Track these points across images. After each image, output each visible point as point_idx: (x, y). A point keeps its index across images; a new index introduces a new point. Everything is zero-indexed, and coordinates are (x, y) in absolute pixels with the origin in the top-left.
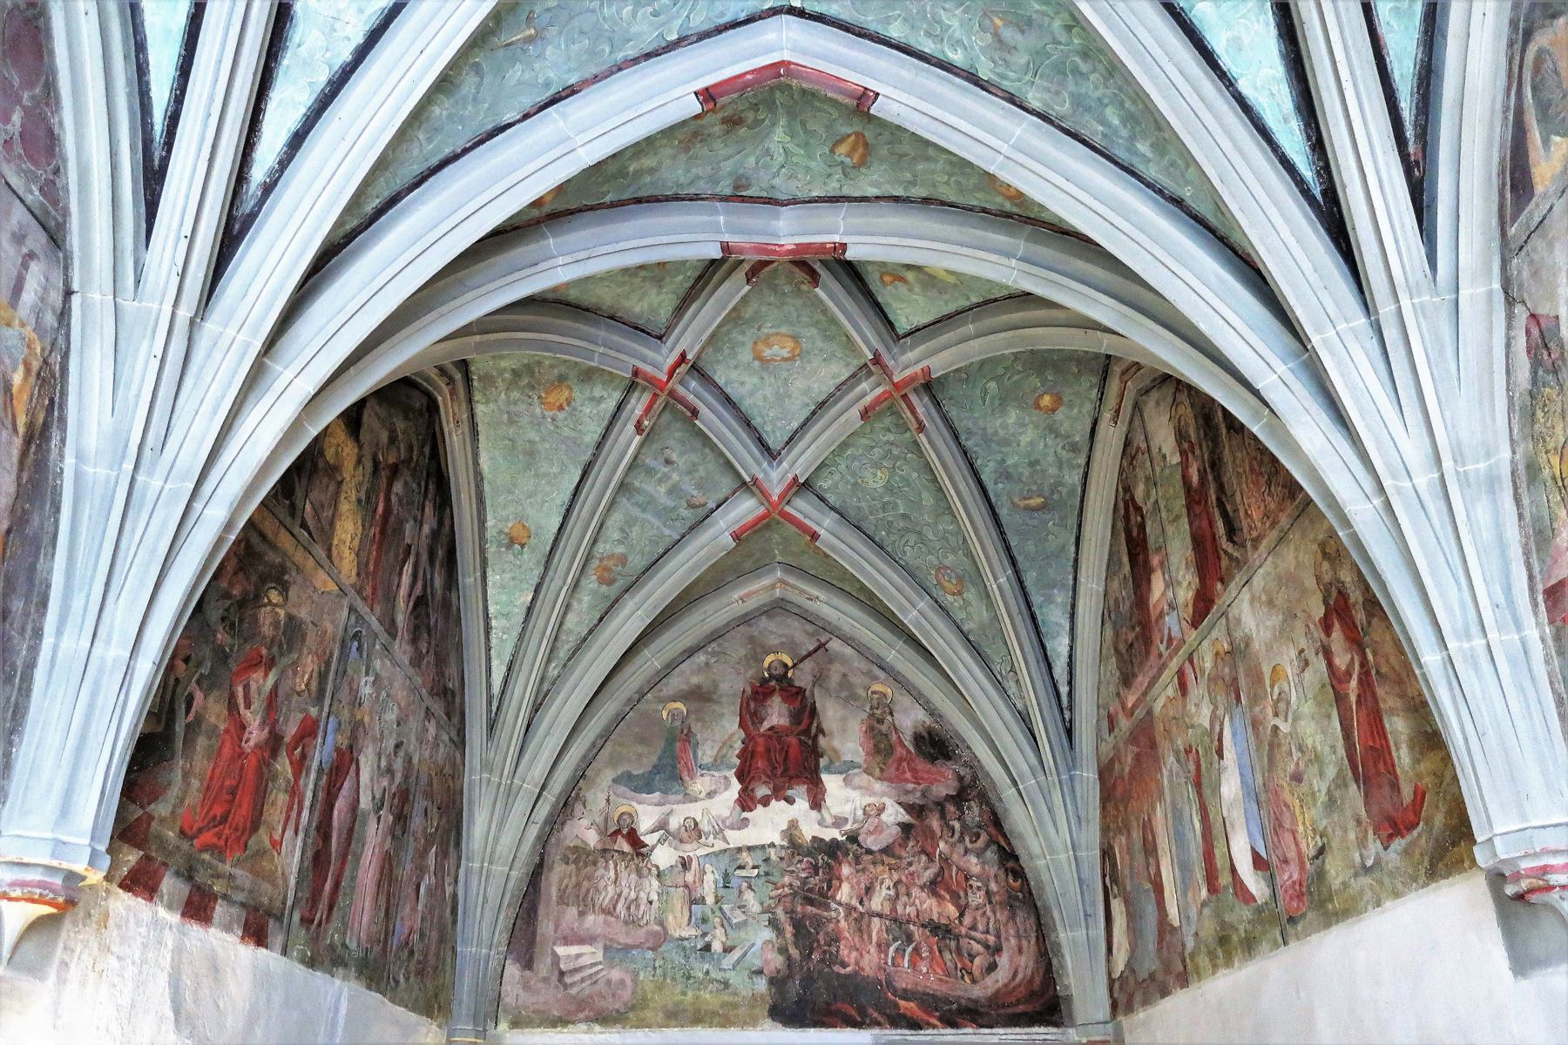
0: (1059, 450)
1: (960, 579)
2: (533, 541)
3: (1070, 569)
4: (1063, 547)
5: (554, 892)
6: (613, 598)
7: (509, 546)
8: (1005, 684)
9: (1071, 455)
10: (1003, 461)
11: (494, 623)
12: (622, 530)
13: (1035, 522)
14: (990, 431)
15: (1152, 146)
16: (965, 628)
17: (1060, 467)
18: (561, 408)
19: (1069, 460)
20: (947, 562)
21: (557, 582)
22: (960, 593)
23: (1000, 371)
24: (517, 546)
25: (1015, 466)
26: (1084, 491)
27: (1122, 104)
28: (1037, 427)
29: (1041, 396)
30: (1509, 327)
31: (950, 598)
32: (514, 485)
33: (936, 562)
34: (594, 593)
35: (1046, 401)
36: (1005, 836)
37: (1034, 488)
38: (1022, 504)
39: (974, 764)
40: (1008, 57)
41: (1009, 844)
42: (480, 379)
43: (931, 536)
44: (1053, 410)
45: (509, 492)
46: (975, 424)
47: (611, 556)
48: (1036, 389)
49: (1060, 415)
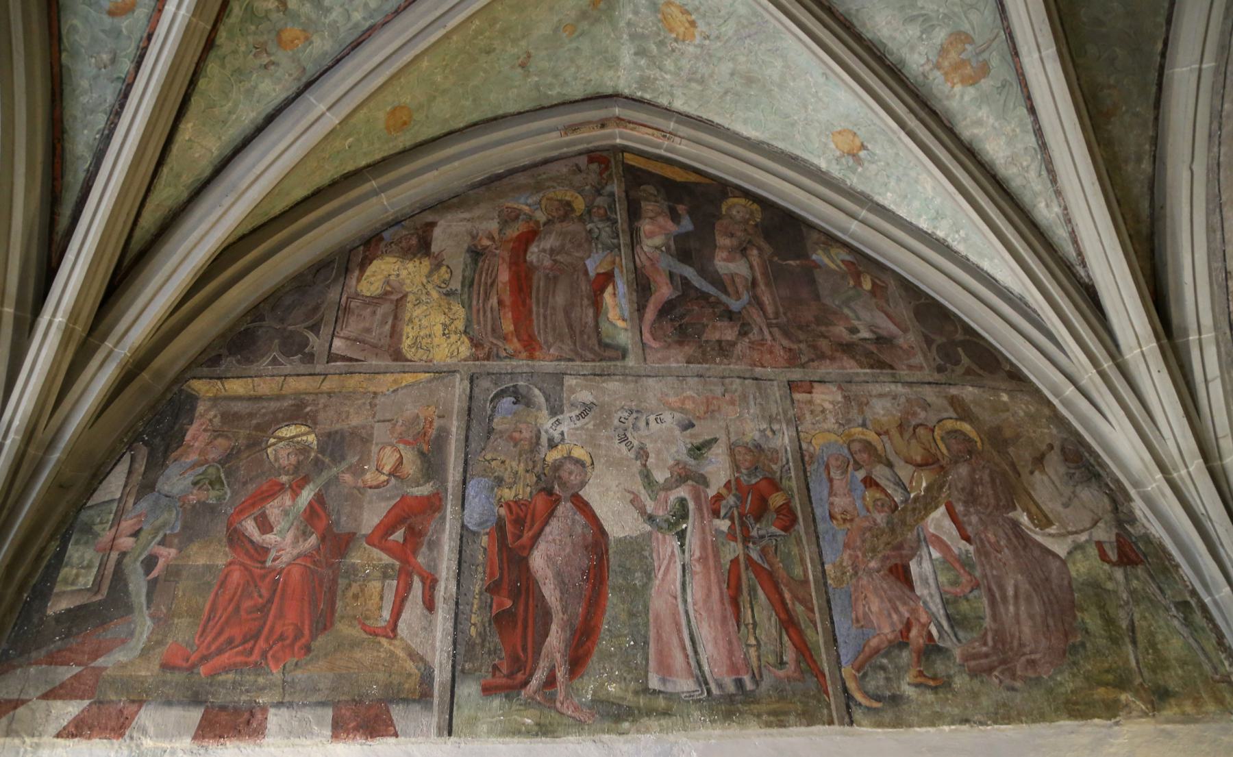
2: (862, 133)
5: (391, 145)
6: (1011, 77)
7: (859, 161)
11: (940, 234)
12: (912, 19)
18: (693, 24)
21: (684, 146)
24: (862, 154)
32: (787, 116)
34: (983, 99)
42: (644, 89)
45: (793, 125)
47: (943, 51)
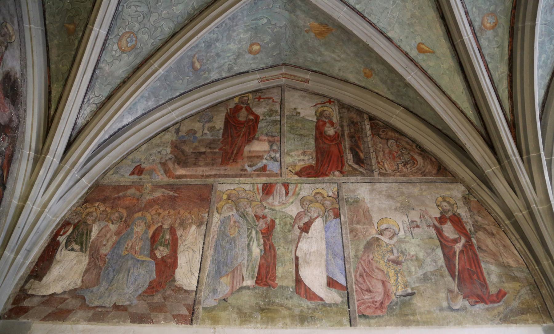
0: (227, 64)
1: (134, 47)
3: (167, 99)
4: (176, 90)
8: (85, 106)
9: (226, 70)
10: (217, 40)
13: (187, 70)
14: (235, 28)
15: (542, 74)
16: (101, 65)
17: (218, 68)
19: (223, 70)
20: (140, 36)
22: (123, 52)
23: (273, 23)
25: (216, 47)
26: (209, 83)
27: (548, 59)
28: (239, 49)
29: (259, 44)
30: (27, 165)
31: (116, 47)
33: (136, 29)
35: (256, 48)
36: (8, 172)
37: (205, 61)
38: (195, 60)
39: (21, 119)
40: (548, 12)
41: (7, 177)
43: (152, 19)
44: (251, 53)
46: (240, 19)
48: (263, 41)
49: (248, 56)
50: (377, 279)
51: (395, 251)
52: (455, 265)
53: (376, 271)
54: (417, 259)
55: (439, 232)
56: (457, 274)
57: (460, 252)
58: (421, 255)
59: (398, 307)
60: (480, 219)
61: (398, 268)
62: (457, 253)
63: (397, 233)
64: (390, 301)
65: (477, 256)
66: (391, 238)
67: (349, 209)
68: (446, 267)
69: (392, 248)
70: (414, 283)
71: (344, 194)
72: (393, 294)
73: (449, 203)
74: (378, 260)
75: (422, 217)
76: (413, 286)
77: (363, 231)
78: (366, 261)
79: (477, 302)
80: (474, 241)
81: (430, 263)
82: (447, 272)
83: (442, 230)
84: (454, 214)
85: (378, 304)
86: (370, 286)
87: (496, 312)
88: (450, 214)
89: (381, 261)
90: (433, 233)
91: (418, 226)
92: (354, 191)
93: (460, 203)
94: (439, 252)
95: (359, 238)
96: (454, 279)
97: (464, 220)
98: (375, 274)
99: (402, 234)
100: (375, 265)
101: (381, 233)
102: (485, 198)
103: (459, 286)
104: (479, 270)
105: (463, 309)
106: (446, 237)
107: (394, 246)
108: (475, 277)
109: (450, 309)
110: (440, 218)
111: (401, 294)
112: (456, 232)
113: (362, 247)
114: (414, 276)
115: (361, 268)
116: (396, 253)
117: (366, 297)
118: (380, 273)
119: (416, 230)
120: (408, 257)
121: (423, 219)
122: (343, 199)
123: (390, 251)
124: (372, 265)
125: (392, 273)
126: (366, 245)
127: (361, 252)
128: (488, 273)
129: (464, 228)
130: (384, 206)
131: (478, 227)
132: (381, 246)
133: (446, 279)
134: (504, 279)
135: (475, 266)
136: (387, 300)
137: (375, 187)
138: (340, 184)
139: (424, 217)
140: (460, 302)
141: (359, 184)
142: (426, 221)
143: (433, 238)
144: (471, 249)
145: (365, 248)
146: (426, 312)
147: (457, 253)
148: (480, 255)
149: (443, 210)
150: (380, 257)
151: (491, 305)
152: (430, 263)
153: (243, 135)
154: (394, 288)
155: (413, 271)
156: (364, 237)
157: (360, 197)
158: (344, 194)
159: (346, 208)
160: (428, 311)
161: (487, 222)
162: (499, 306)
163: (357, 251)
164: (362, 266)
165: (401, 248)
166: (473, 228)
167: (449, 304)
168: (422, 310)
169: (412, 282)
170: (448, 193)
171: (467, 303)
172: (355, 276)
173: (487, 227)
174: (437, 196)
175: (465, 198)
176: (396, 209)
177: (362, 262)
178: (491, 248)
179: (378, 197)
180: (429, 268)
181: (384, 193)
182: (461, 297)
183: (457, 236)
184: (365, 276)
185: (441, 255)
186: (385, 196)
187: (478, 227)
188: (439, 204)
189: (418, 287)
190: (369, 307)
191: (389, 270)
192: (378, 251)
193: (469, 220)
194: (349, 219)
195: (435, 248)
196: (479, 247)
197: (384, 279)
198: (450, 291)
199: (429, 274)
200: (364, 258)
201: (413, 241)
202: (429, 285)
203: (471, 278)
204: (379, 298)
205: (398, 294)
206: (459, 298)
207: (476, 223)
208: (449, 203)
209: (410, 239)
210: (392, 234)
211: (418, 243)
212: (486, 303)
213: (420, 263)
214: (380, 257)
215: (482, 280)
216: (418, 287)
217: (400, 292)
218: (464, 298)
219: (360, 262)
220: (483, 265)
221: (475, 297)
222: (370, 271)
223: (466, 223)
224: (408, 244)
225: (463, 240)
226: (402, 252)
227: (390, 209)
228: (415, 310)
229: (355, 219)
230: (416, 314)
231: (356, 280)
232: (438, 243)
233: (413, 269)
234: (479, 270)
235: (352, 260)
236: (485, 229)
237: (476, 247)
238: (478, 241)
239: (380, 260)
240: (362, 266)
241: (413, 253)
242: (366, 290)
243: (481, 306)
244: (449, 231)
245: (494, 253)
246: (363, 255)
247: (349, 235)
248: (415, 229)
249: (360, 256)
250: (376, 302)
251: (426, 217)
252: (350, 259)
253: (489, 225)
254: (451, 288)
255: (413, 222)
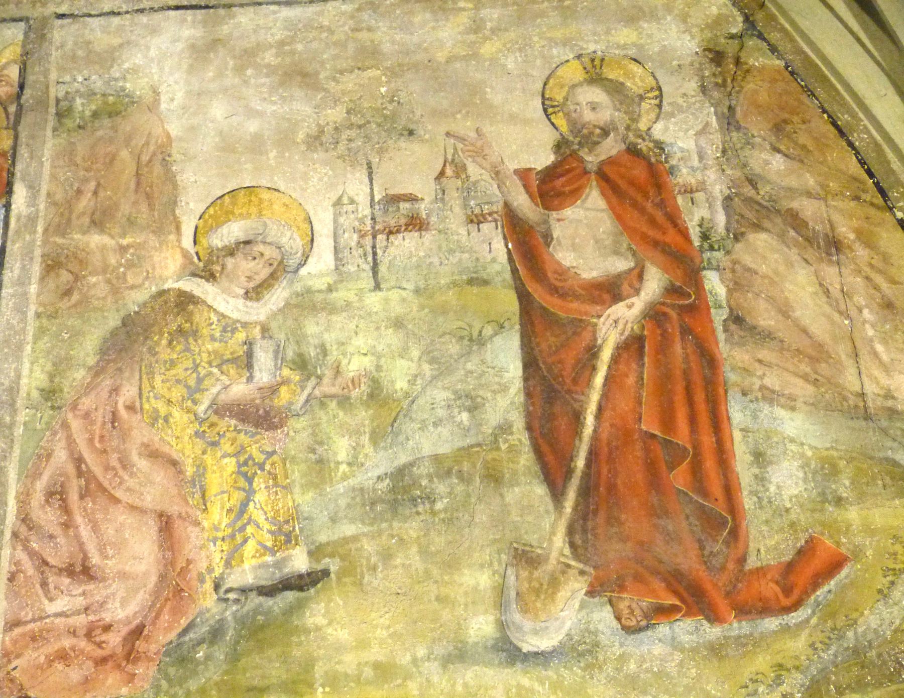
50: (133, 508)
51: (264, 359)
52: (577, 418)
53: (142, 464)
54: (376, 393)
55: (528, 246)
56: (580, 463)
57: (622, 349)
58: (399, 377)
59: (220, 654)
60: (777, 163)
61: (257, 445)
62: (606, 355)
63: (293, 262)
64: (184, 622)
65: (711, 361)
66: (255, 293)
67: (67, 154)
68: (529, 428)
69: (249, 344)
70: (334, 520)
71: (59, 78)
72: (209, 586)
73: (616, 89)
74: (163, 410)
75: (451, 170)
76: (323, 538)
77: (113, 260)
78: (99, 417)
79: (662, 612)
80: (715, 284)
81: (441, 413)
82: (526, 459)
83: (548, 237)
84: (633, 151)
85: (114, 640)
86: (91, 548)
87: (762, 662)
88: (611, 147)
89: (177, 415)
90: (494, 249)
91: (416, 224)
92: (105, 59)
93: (682, 88)
94: (506, 357)
95: (85, 301)
96: (557, 495)
97: (684, 176)
98: (131, 482)
99: (319, 267)
100: (140, 433)
101: (208, 269)
102: (829, 50)
103: (580, 532)
104: (707, 440)
105: (580, 650)
106: (562, 272)
107: (265, 330)
108: (679, 478)
109: (508, 651)
110: (549, 174)
111: (249, 579)
112: (625, 242)
113: (88, 349)
114: (341, 488)
115: (61, 455)
116: (265, 369)
117: (60, 604)
118: (161, 476)
119: (406, 245)
120: (327, 387)
121: (452, 184)
122: (42, 103)
123: (234, 360)
124: (125, 436)
125: (221, 472)
126: (114, 333)
127: (80, 374)
128: (759, 457)
129: (674, 220)
130: (253, 126)
131: (752, 208)
132: (195, 333)
133: (512, 495)
134: (844, 486)
135: (693, 420)
136: (166, 616)
137: (225, 29)
138: (44, 22)
139: (460, 170)
140: (571, 612)
141: (144, 19)
142: (469, 190)
143: (485, 283)
144: (686, 331)
145: (103, 351)
146: (368, 672)
147: (606, 355)
148: (732, 355)
149: (576, 127)
150: (177, 393)
151: (738, 627)
152: (441, 413)
153: (778, 597)
154: (217, 554)
155: (342, 456)
156: (115, 291)
157: (136, 86)
158: (53, 76)
159: (50, 145)
160: (377, 666)
161: (811, 181)
162: (786, 629)
163: (60, 366)
164: (71, 442)
165: (300, 338)
166: (721, 219)
167: (502, 626)
168: (349, 662)
169: (323, 518)
170: (625, 35)
171: (603, 617)
172: (24, 501)
173: (808, 208)
174: (559, 53)
175: (717, 57)
176: (315, 141)
177: (75, 424)
178: (806, 321)
179: (231, 80)
180: (429, 441)
181: (269, 57)
182: (575, 587)
183: (621, 265)
184: (73, 497)
185: (514, 369)
186: (271, 70)
187: (752, 208)
188: (559, 98)
189: (346, 540)
190: (63, 656)
191: (208, 459)
192: (173, 364)
193: (712, 175)
194: (52, 203)
195: (488, 331)
196: (736, 319)
197: (174, 509)
198: (525, 557)
199: (423, 470)
200: (87, 403)
201: (374, 300)
202: (412, 529)
203: (655, 481)
204: (122, 608)
205: (234, 580)
206: (563, 594)
207: (748, 191)
208: (616, 89)
209: (360, 294)
210: (265, 273)
211: (397, 309)
212: (714, 617)
213: (384, 408)
214: (177, 393)
215: (717, 490)
216: (355, 538)
217: (246, 573)
218: (591, 593)
219: (65, 425)
220: (737, 413)
221: (658, 585)
222: (107, 468)
223: (689, 191)
224: (338, 319)
225: (654, 283)
226: (302, 364)
227: (285, 140)
228: (308, 665)
229: (85, 203)
230: (311, 686)
231: (25, 519)
232: (510, 303)
233: (341, 448)
234: (707, 440)
235: (23, 416)
236: (795, 220)
237: (719, 317)
238: (736, 287)
239: (169, 404)
240: (71, 442)
241: (355, 365)
242: (70, 571)
243: (687, 630)
244: (585, 238)
245: (820, 346)
246: (89, 388)
247: (33, 288)
248: (396, 240)
249: (68, 394)
250: (107, 628)
251: (473, 170)
252: (14, 412)
253: (823, 195)
254: (533, 539)
255: (394, 200)
